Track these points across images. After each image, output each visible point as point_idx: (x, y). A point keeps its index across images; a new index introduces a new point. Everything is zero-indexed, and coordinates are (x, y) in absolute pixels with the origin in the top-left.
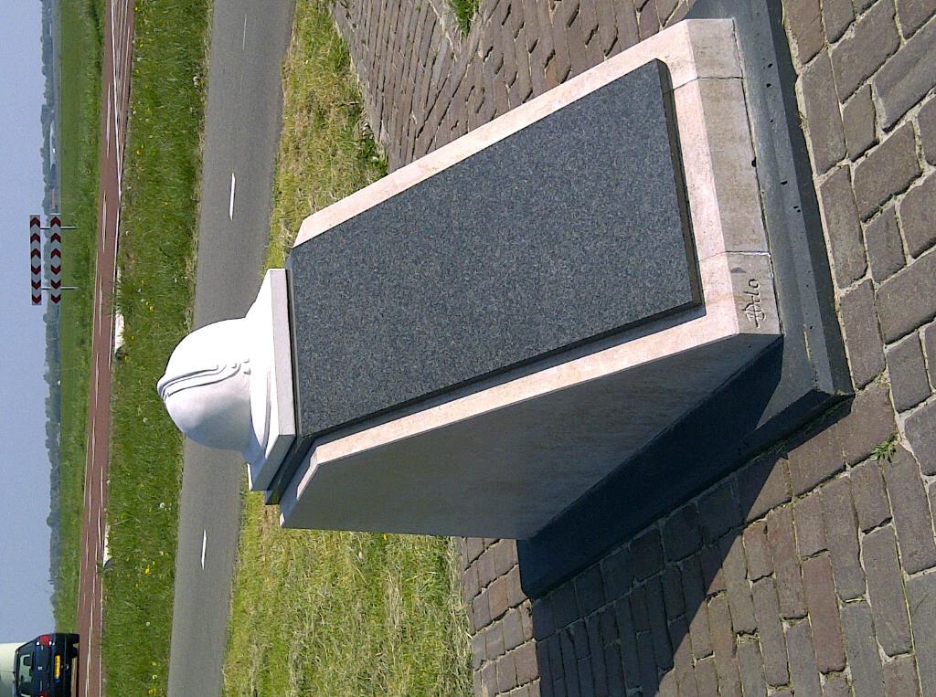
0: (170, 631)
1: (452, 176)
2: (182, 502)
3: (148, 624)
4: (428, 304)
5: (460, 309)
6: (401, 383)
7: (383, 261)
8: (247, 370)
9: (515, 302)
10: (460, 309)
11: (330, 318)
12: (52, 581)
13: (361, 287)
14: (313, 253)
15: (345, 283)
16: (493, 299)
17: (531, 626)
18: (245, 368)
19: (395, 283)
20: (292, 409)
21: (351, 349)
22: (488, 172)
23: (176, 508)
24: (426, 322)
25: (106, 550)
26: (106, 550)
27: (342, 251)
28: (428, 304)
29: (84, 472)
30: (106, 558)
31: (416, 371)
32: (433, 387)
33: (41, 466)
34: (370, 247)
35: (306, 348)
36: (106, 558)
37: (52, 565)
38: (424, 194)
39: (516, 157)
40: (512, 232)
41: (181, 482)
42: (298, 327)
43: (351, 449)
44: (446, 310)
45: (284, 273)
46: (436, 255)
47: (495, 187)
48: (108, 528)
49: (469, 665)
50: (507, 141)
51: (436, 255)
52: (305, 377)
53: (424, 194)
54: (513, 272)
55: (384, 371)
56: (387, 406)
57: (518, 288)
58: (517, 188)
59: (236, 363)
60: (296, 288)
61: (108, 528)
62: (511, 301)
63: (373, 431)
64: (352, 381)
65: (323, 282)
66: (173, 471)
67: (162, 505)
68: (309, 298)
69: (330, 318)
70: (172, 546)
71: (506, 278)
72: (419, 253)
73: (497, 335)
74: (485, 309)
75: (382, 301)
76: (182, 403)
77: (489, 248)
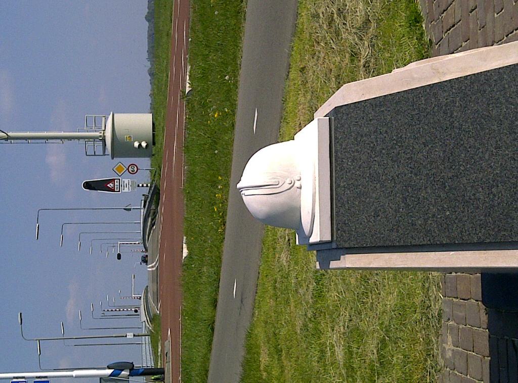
0: (231, 161)
1: (457, 86)
2: (241, 79)
3: (216, 152)
4: (432, 179)
5: (455, 189)
6: (408, 231)
7: (401, 136)
8: (299, 186)
9: (497, 197)
10: (455, 189)
11: (360, 168)
12: (149, 59)
13: (384, 152)
14: (349, 116)
15: (372, 145)
16: (481, 189)
17: (487, 321)
18: (297, 184)
19: (408, 156)
20: (329, 159)
21: (374, 195)
22: (485, 91)
23: (237, 82)
24: (429, 191)
25: (188, 85)
26: (188, 85)
27: (370, 120)
28: (432, 179)
29: (172, 9)
30: (188, 90)
31: (420, 225)
32: (432, 241)
33: (144, 64)
34: (392, 123)
35: (342, 184)
36: (188, 90)
37: (148, 49)
38: (435, 94)
39: (507, 86)
40: (499, 143)
41: (240, 65)
42: (336, 167)
43: (370, 264)
44: (445, 187)
45: (328, 120)
46: (440, 143)
47: (488, 105)
48: (189, 67)
49: (440, 315)
50: (501, 71)
51: (440, 143)
52: (340, 205)
53: (435, 94)
54: (497, 173)
55: (397, 218)
56: (397, 244)
57: (500, 187)
58: (505, 110)
59: (289, 171)
60: (336, 138)
61: (189, 67)
62: (494, 195)
63: (386, 256)
64: (373, 218)
65: (356, 139)
66: (235, 58)
67: (227, 78)
68: (345, 148)
69: (360, 168)
70: (233, 106)
71: (491, 177)
72: (428, 139)
73: (482, 217)
74: (474, 195)
75: (398, 166)
76: (255, 202)
77: (481, 150)
